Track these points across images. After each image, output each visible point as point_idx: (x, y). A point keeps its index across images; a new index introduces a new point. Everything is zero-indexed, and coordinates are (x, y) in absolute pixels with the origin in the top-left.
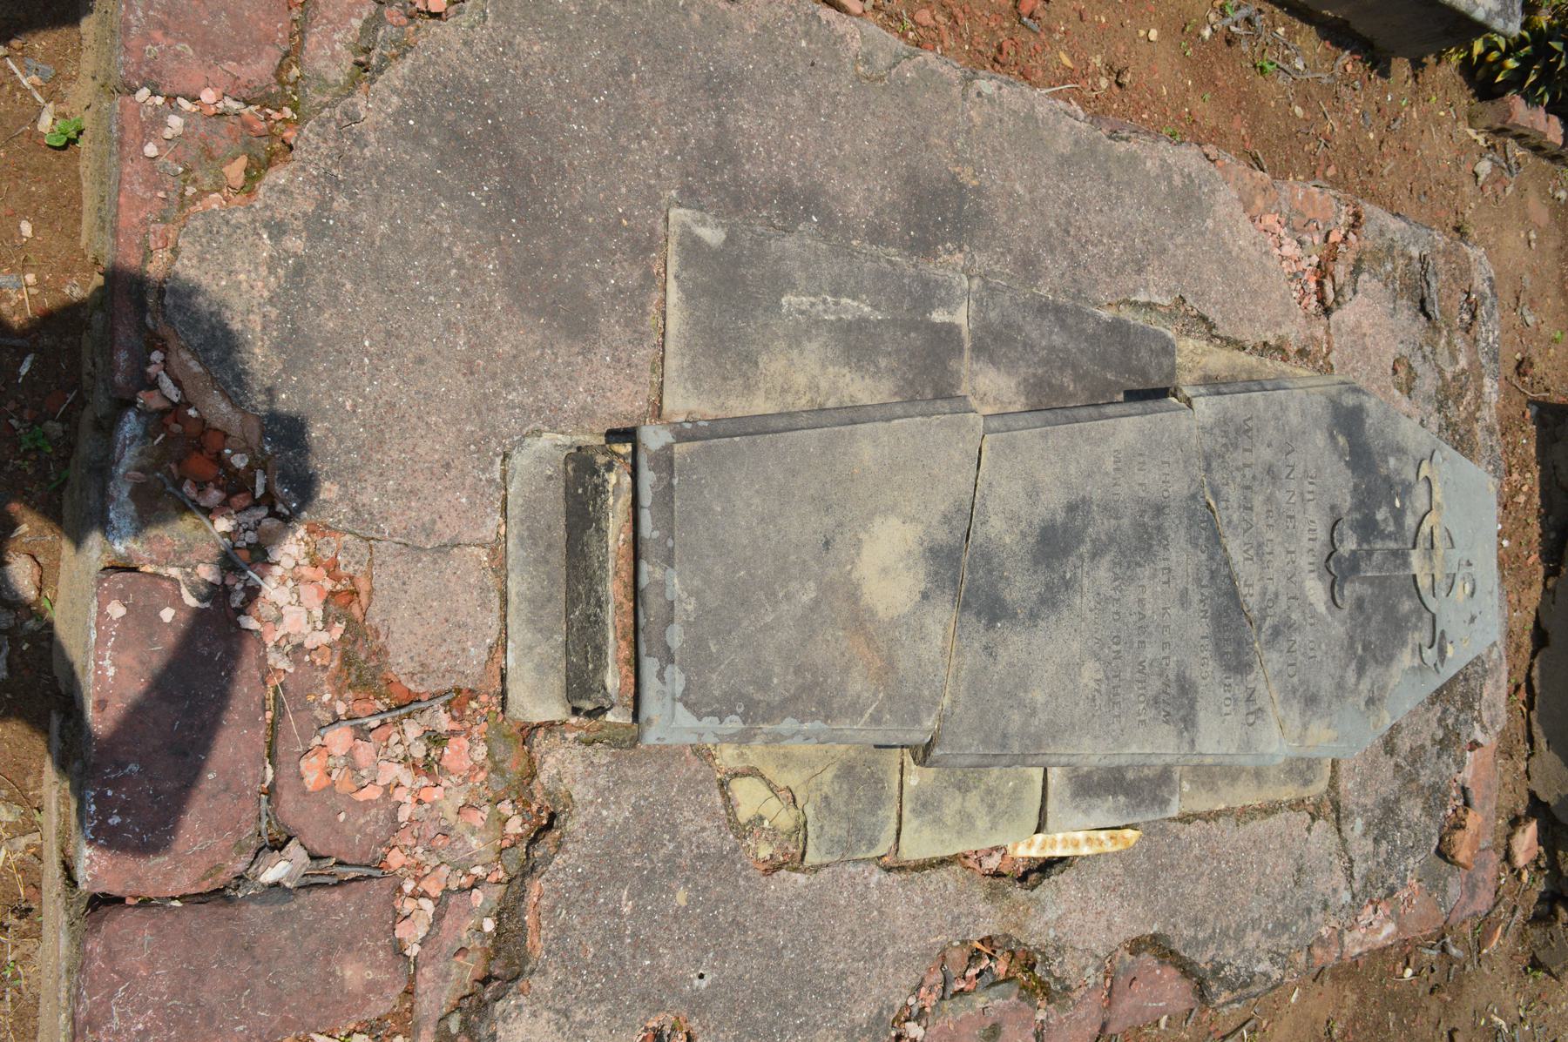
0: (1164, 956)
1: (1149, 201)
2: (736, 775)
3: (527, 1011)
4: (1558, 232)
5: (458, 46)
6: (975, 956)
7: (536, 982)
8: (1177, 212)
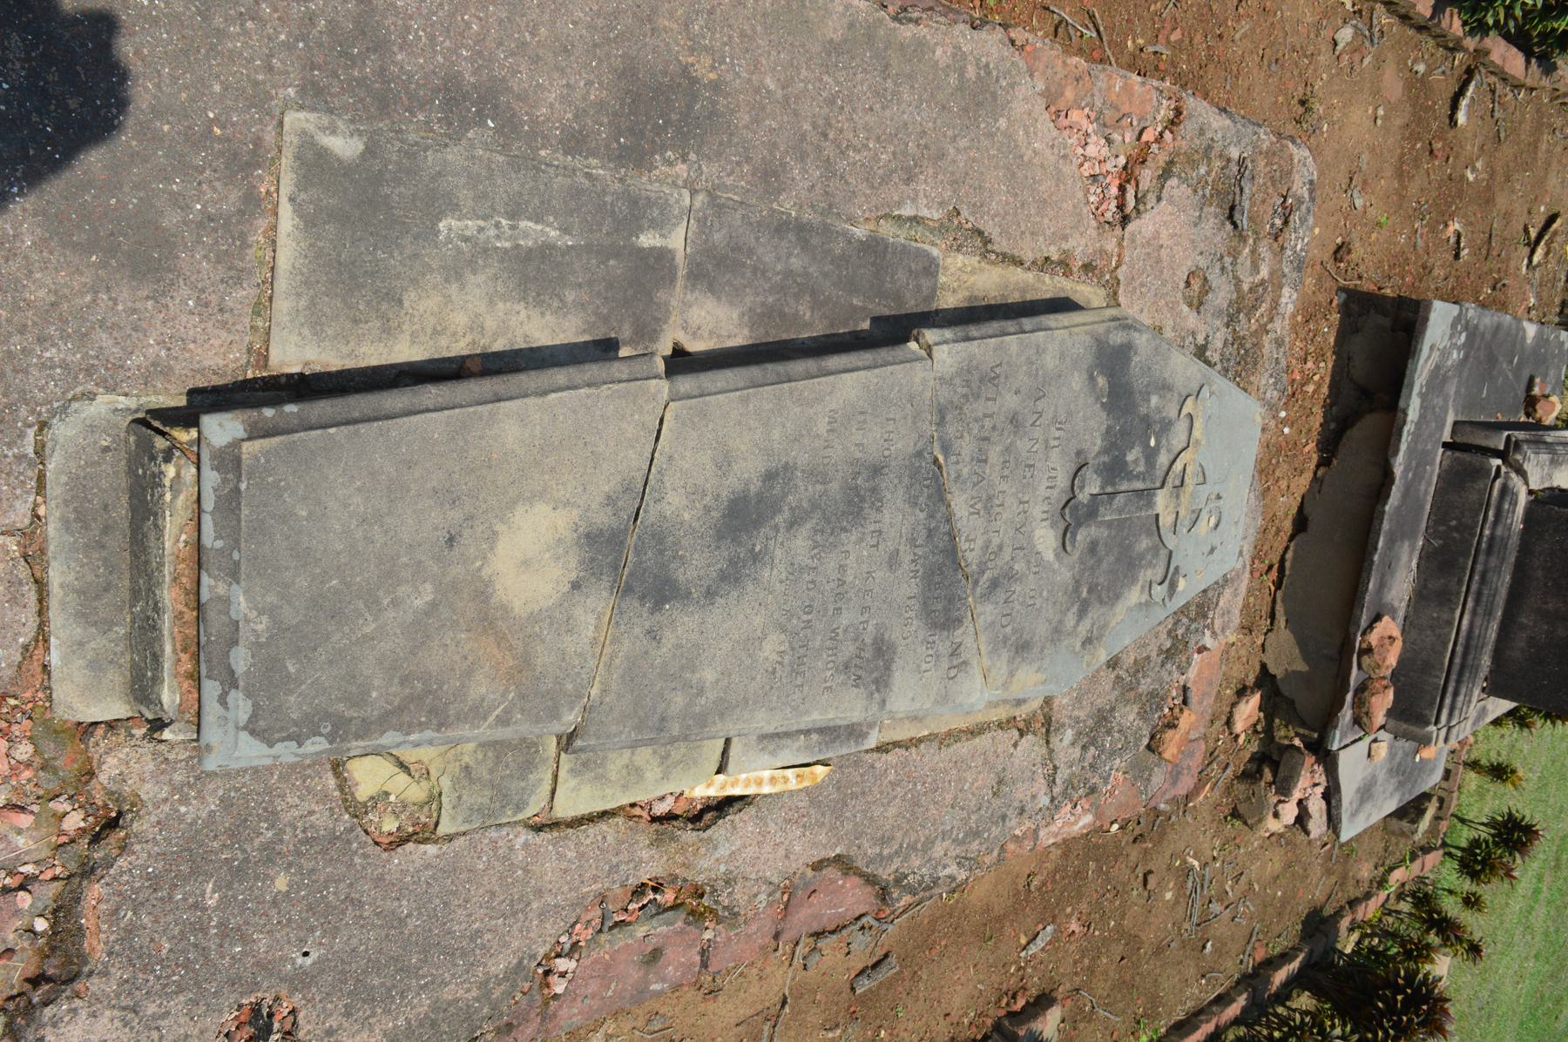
3: (83, 1014)
4: (1409, 109)
7: (95, 984)
8: (965, 110)
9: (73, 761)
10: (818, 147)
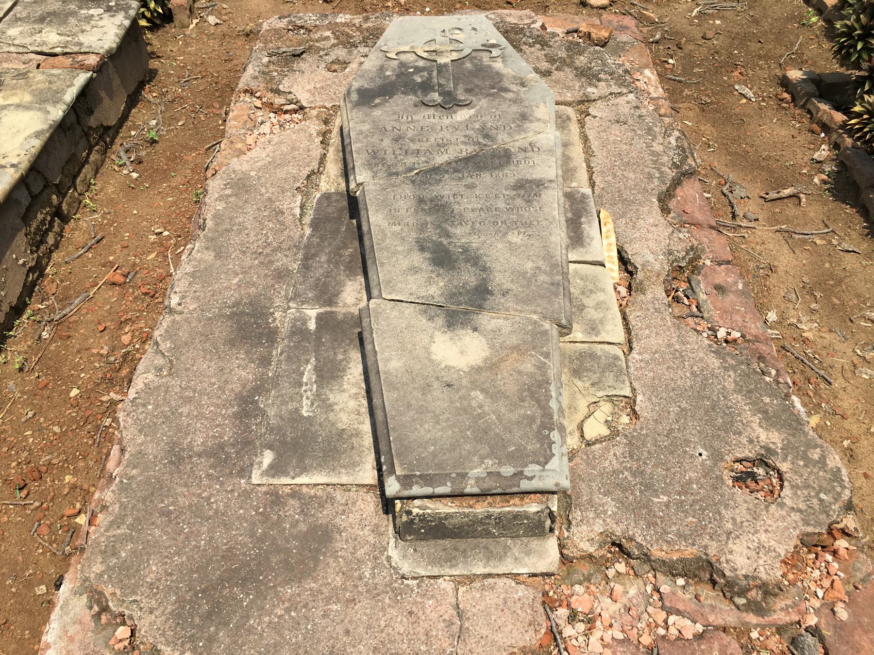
0: (670, 195)
1: (240, 208)
2: (582, 436)
3: (729, 557)
5: (153, 617)
6: (677, 300)
7: (712, 552)
9: (584, 565)
10: (266, 256)
